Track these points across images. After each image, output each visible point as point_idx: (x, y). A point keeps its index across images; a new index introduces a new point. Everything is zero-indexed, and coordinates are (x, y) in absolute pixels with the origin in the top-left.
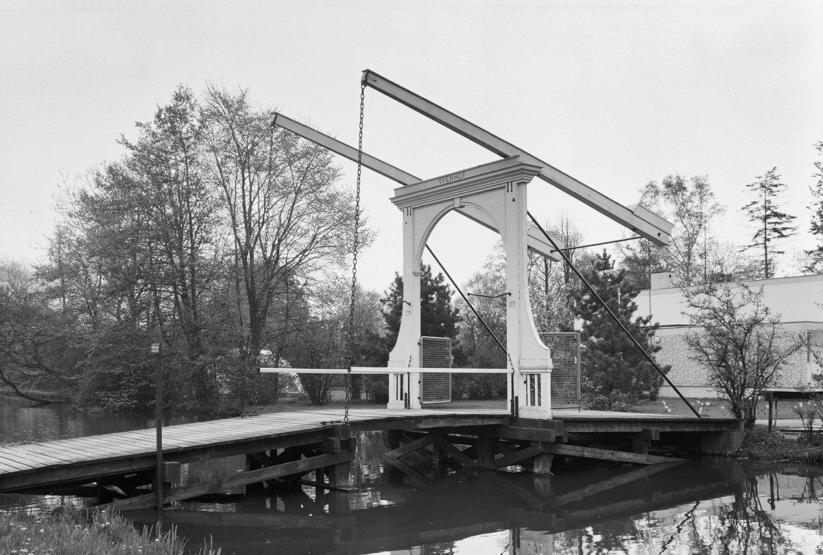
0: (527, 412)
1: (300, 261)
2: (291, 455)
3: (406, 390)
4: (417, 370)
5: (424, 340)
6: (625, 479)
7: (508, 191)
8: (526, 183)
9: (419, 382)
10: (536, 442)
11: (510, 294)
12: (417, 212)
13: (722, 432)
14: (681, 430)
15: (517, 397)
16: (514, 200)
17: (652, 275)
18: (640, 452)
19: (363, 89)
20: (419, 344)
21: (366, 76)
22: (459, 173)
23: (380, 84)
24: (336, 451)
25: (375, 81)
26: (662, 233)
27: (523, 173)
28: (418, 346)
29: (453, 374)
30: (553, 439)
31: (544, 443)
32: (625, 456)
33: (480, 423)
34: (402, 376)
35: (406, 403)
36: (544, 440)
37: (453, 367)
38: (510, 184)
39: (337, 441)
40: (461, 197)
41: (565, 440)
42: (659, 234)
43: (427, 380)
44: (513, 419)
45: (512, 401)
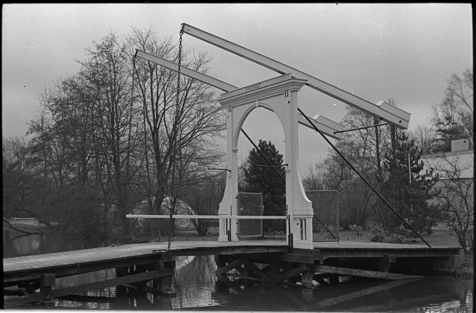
0: (298, 244)
1: (192, 136)
2: (141, 269)
3: (229, 229)
4: (236, 217)
5: (240, 195)
6: (371, 291)
7: (286, 96)
8: (297, 91)
9: (237, 223)
10: (303, 264)
11: (287, 165)
12: (235, 109)
13: (448, 257)
14: (415, 256)
15: (292, 234)
16: (289, 102)
17: (452, 141)
18: (383, 271)
19: (181, 36)
20: (236, 198)
21: (183, 27)
22: (257, 84)
23: (192, 31)
24: (161, 269)
25: (189, 30)
26: (402, 121)
27: (294, 85)
28: (237, 199)
29: (264, 220)
30: (312, 262)
31: (306, 264)
32: (370, 274)
33: (266, 251)
34: (227, 219)
35: (228, 237)
36: (306, 263)
37: (264, 215)
38: (287, 91)
39: (161, 263)
40: (259, 100)
41: (322, 262)
42: (400, 122)
43: (240, 222)
44: (290, 248)
45: (289, 236)
